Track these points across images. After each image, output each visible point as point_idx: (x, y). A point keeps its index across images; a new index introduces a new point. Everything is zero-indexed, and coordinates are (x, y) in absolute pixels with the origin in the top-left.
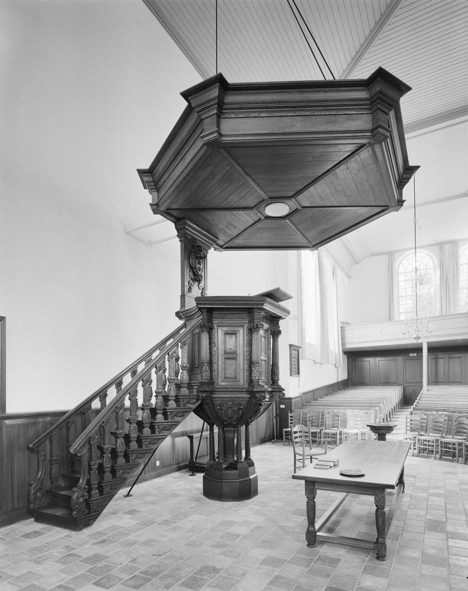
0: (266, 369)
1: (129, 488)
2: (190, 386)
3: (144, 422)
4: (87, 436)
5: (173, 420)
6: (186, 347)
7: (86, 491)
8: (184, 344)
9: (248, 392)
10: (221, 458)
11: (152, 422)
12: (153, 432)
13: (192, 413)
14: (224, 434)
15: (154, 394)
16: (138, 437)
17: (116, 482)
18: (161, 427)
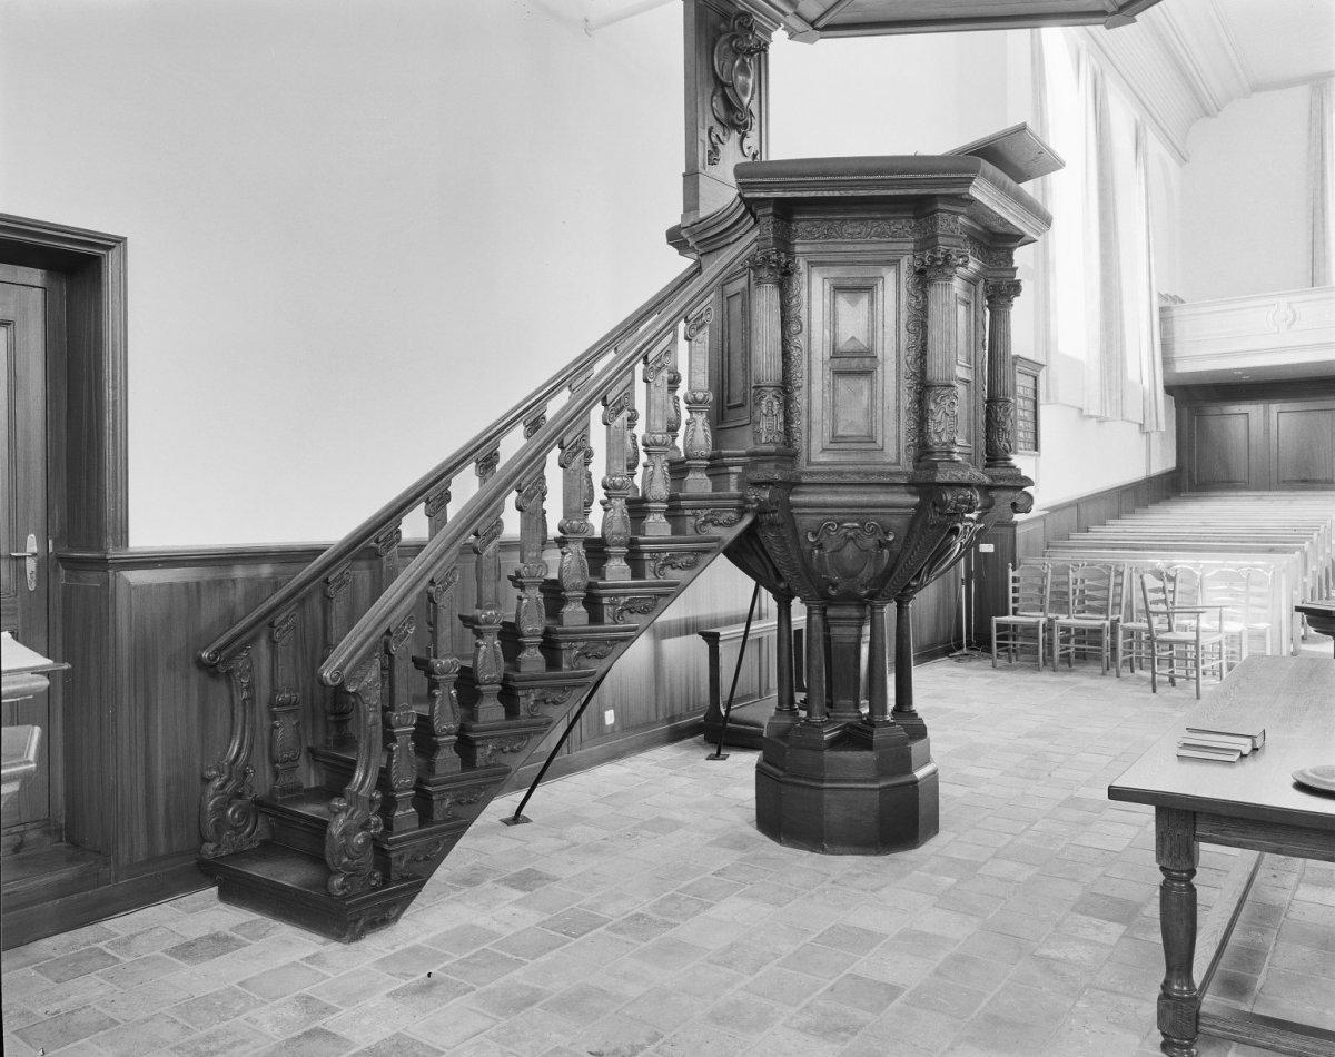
0: (969, 412)
1: (521, 795)
2: (716, 466)
3: (567, 584)
4: (379, 624)
5: (662, 580)
6: (704, 336)
7: (377, 807)
8: (696, 326)
9: (913, 485)
10: (816, 708)
11: (590, 586)
12: (595, 617)
13: (722, 555)
14: (827, 628)
15: (600, 494)
16: (547, 632)
17: (473, 782)
18: (622, 600)
